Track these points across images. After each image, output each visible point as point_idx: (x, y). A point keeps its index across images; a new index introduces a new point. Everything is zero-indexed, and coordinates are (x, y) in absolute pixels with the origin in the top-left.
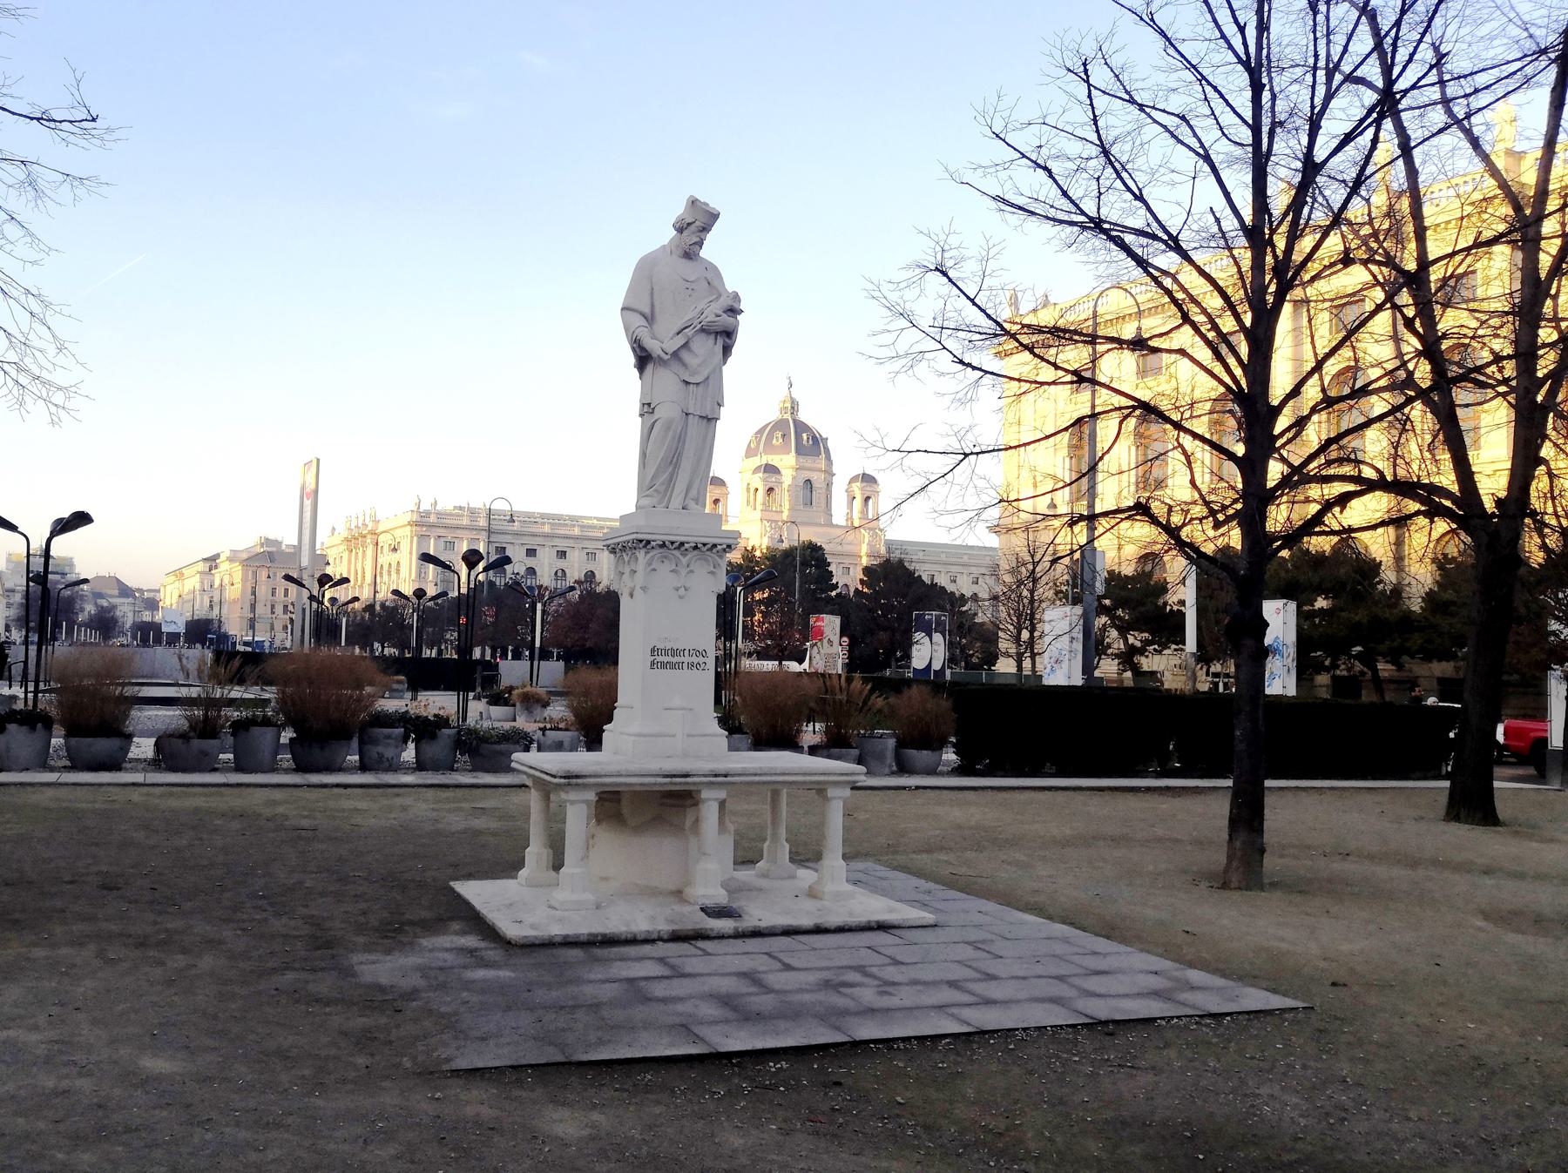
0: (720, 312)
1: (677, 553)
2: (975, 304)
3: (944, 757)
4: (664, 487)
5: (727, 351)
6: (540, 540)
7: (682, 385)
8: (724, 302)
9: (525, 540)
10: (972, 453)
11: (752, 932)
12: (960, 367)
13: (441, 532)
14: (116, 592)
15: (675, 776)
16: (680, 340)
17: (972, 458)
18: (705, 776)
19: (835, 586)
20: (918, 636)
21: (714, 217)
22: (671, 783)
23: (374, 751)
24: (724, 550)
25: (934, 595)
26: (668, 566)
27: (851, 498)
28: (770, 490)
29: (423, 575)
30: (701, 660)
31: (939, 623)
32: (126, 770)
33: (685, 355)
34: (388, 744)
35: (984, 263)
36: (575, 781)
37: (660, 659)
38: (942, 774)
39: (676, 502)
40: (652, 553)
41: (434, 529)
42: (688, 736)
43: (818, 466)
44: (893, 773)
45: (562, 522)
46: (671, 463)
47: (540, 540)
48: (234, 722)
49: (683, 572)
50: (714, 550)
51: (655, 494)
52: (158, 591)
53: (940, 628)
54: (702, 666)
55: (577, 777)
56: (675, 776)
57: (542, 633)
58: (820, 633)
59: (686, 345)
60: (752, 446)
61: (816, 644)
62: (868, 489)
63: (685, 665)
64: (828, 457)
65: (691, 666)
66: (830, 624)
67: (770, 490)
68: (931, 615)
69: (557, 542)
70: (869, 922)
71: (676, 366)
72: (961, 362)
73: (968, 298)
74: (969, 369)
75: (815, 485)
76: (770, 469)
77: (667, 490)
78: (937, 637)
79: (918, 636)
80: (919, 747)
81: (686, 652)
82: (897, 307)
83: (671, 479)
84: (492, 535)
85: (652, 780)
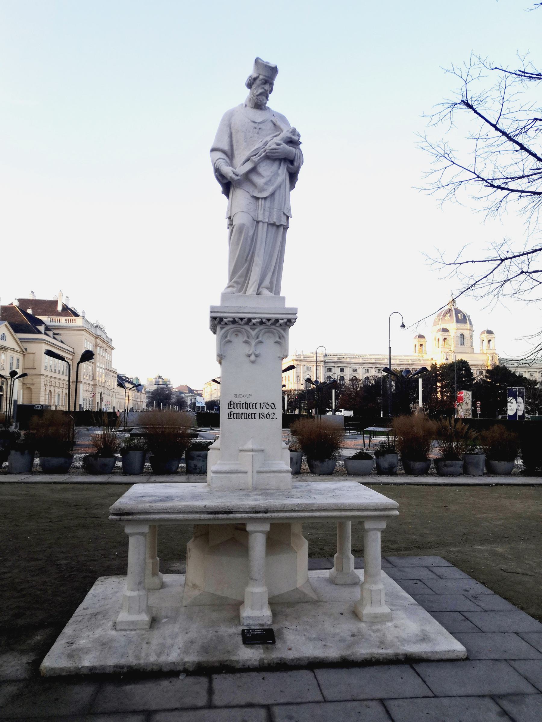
0: (279, 142)
1: (247, 328)
2: (497, 129)
3: (516, 462)
4: (243, 279)
5: (293, 177)
6: (345, 365)
7: (252, 200)
8: (285, 134)
9: (339, 365)
10: (507, 259)
11: (277, 664)
12: (492, 190)
13: (305, 363)
14: (187, 391)
15: (218, 513)
16: (249, 166)
17: (507, 262)
18: (247, 512)
19: (474, 379)
20: (509, 399)
21: (274, 71)
22: (215, 519)
23: (192, 463)
24: (286, 323)
25: (520, 380)
26: (241, 338)
27: (482, 341)
28: (445, 339)
29: (298, 381)
30: (270, 411)
31: (520, 392)
32: (74, 473)
33: (255, 179)
34: (200, 460)
35: (503, 90)
36: (125, 517)
37: (236, 411)
38: (515, 475)
39: (251, 290)
40: (227, 328)
41: (302, 362)
42: (259, 472)
43: (466, 328)
44: (484, 475)
45: (354, 357)
46: (246, 260)
47: (345, 365)
48: (122, 448)
49: (253, 343)
50: (278, 324)
51: (235, 285)
52: (202, 391)
53: (521, 395)
54: (272, 416)
55: (129, 514)
56: (218, 513)
57: (335, 404)
58: (461, 400)
59: (254, 170)
60: (436, 320)
61: (459, 405)
62: (490, 336)
63: (257, 416)
64: (471, 324)
65: (262, 416)
66: (467, 395)
67: (445, 339)
68: (516, 389)
69: (352, 365)
70: (397, 655)
71: (248, 187)
72: (492, 186)
73: (491, 124)
74: (499, 190)
75: (465, 336)
76: (445, 330)
77: (245, 280)
78: (520, 399)
79: (509, 399)
80: (500, 460)
81: (258, 406)
82: (438, 149)
83: (248, 271)
84: (318, 363)
85: (197, 516)
